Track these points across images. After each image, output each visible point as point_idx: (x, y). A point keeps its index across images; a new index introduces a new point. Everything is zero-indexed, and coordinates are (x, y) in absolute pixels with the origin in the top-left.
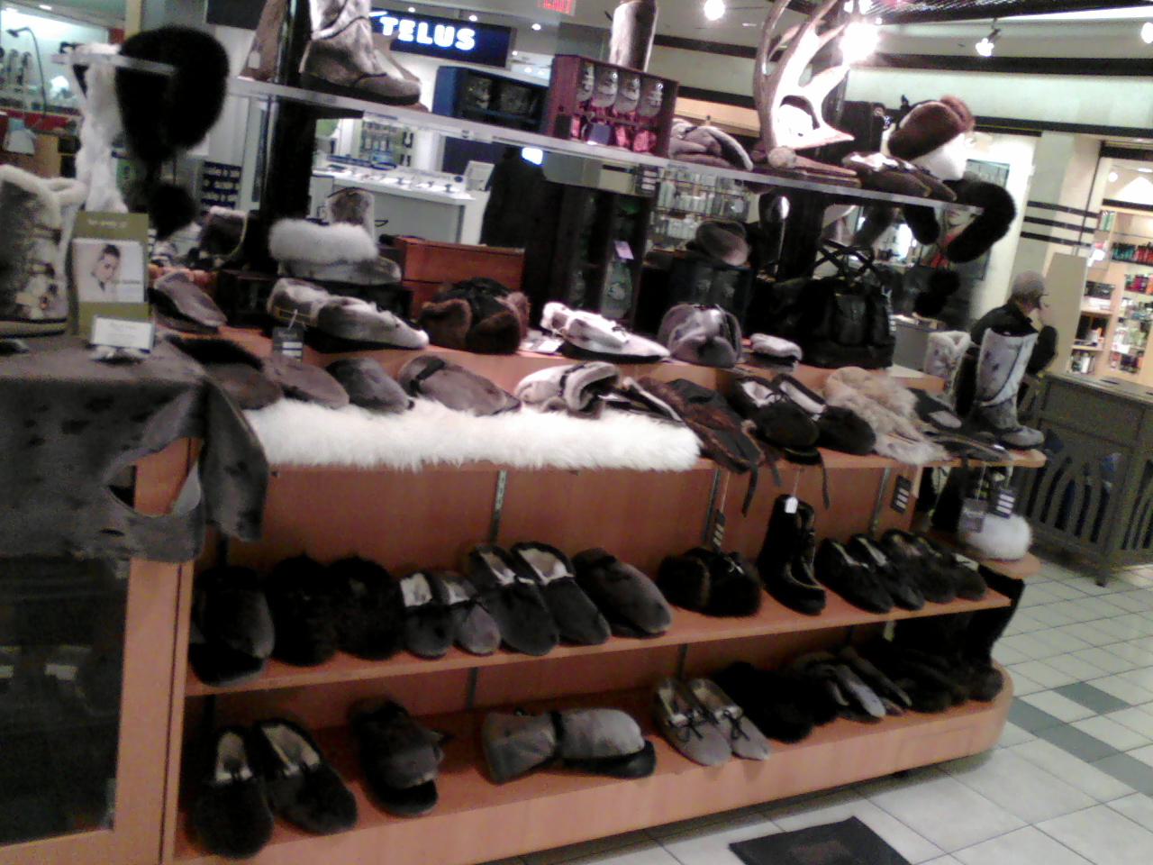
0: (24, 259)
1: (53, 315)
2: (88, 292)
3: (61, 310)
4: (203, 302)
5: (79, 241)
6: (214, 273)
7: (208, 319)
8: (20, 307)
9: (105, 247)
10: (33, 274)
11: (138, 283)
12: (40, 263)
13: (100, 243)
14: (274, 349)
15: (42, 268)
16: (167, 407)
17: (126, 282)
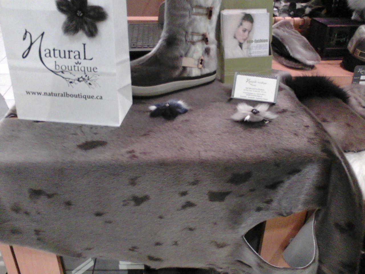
0: (187, 33)
1: (207, 71)
2: (232, 51)
3: (212, 65)
4: (305, 47)
5: (225, 12)
6: (306, 18)
7: (308, 60)
8: (185, 68)
9: (243, 15)
10: (193, 43)
11: (265, 41)
12: (198, 34)
13: (238, 13)
14: (354, 80)
15: (200, 38)
16: (294, 178)
17: (257, 41)
